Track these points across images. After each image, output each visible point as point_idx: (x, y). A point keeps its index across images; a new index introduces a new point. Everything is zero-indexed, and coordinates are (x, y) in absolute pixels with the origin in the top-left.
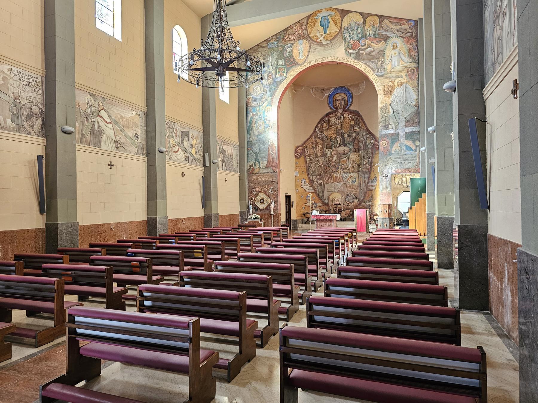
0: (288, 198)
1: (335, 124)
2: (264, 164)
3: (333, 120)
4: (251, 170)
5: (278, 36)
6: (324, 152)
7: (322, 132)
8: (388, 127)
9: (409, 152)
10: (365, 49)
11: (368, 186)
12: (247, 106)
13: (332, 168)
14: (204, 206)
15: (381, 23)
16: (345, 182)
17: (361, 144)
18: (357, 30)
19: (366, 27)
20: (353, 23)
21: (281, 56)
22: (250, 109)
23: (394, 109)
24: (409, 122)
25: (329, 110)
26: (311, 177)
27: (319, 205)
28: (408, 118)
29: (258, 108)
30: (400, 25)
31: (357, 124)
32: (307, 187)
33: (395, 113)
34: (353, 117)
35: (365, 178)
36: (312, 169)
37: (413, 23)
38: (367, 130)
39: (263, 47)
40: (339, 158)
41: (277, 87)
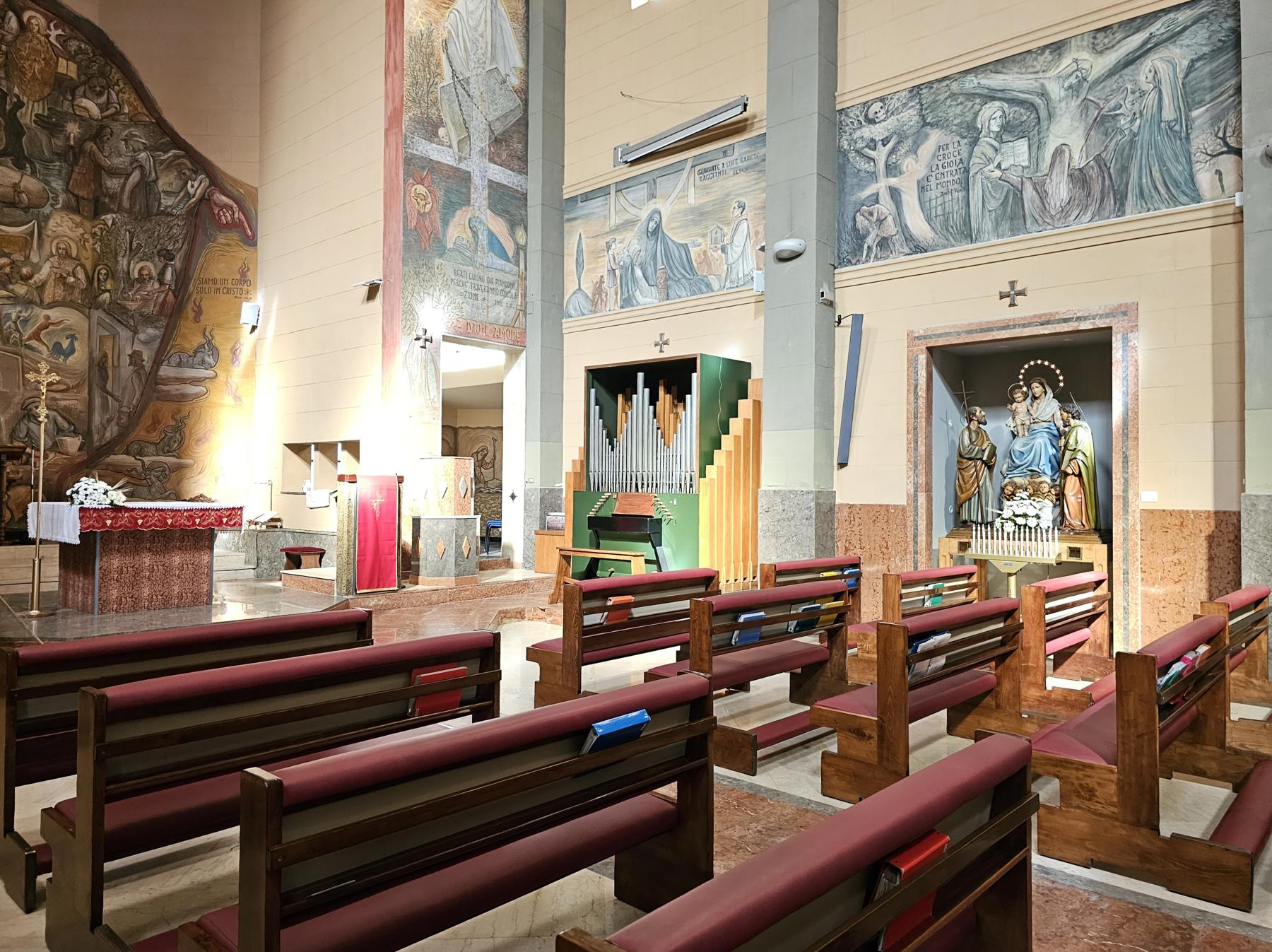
0: (634, 162)
8: (436, 135)
11: (151, 381)
23: (458, 69)
28: (499, 128)
31: (91, 83)
33: (459, 86)
34: (73, 45)
35: (134, 344)
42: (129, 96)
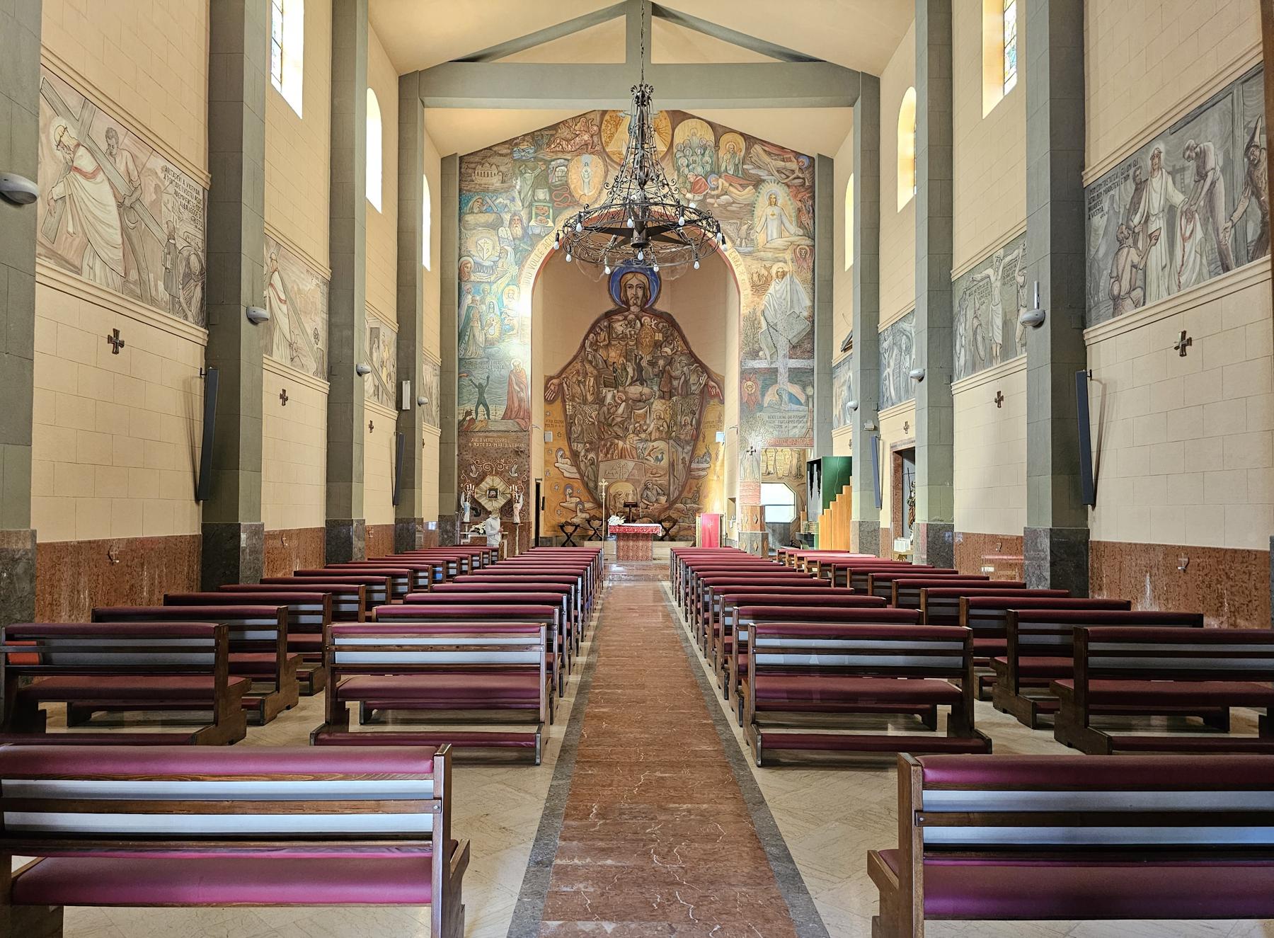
0: (538, 486)
1: (624, 337)
2: (498, 411)
3: (619, 327)
4: (466, 424)
5: (541, 138)
6: (599, 392)
7: (596, 351)
9: (795, 407)
10: (718, 197)
12: (460, 279)
13: (616, 428)
14: (396, 502)
15: (748, 149)
16: (641, 459)
17: (675, 383)
18: (703, 155)
19: (721, 154)
20: (695, 141)
21: (542, 181)
22: (466, 286)
24: (796, 349)
25: (610, 306)
26: (575, 446)
27: (588, 505)
28: (795, 341)
29: (487, 287)
30: (783, 160)
31: (668, 340)
32: (565, 466)
35: (684, 453)
36: (576, 429)
37: (806, 162)
38: (692, 354)
39: (501, 155)
40: (631, 409)
41: (533, 246)
42: (681, 342)
